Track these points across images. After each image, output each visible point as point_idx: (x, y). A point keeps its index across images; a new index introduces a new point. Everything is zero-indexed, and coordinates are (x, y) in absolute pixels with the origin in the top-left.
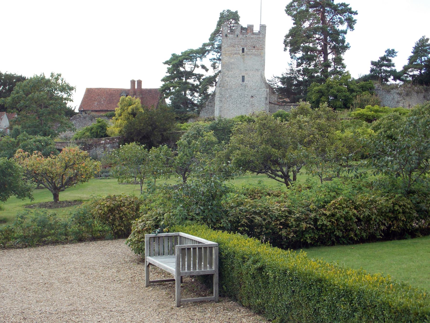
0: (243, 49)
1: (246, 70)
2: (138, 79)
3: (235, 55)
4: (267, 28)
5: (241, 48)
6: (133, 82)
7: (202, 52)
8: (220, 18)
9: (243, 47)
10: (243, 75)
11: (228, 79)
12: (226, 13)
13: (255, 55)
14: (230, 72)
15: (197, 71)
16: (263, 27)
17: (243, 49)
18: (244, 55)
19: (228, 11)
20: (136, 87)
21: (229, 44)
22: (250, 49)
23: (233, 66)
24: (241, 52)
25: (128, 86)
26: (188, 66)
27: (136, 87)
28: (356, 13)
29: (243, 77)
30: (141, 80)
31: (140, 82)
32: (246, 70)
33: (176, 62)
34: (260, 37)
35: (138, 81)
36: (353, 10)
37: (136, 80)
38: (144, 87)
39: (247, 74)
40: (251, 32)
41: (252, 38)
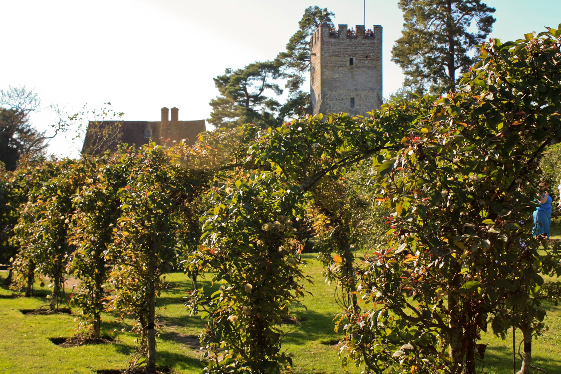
0: (351, 60)
1: (356, 90)
2: (172, 107)
3: (340, 69)
4: (383, 30)
5: (349, 59)
6: (165, 111)
7: (274, 68)
8: (305, 16)
9: (351, 57)
10: (352, 97)
11: (330, 102)
12: (313, 10)
13: (368, 68)
14: (334, 93)
15: (269, 94)
16: (378, 29)
17: (351, 60)
18: (352, 68)
19: (317, 8)
20: (170, 119)
21: (331, 52)
22: (361, 60)
23: (338, 84)
24: (348, 63)
25: (157, 117)
26: (253, 87)
27: (170, 119)
28: (493, 10)
29: (353, 100)
30: (177, 107)
31: (175, 111)
32: (356, 90)
34: (374, 43)
35: (172, 110)
36: (489, 6)
37: (170, 107)
38: (182, 117)
39: (357, 95)
40: (361, 35)
41: (363, 44)
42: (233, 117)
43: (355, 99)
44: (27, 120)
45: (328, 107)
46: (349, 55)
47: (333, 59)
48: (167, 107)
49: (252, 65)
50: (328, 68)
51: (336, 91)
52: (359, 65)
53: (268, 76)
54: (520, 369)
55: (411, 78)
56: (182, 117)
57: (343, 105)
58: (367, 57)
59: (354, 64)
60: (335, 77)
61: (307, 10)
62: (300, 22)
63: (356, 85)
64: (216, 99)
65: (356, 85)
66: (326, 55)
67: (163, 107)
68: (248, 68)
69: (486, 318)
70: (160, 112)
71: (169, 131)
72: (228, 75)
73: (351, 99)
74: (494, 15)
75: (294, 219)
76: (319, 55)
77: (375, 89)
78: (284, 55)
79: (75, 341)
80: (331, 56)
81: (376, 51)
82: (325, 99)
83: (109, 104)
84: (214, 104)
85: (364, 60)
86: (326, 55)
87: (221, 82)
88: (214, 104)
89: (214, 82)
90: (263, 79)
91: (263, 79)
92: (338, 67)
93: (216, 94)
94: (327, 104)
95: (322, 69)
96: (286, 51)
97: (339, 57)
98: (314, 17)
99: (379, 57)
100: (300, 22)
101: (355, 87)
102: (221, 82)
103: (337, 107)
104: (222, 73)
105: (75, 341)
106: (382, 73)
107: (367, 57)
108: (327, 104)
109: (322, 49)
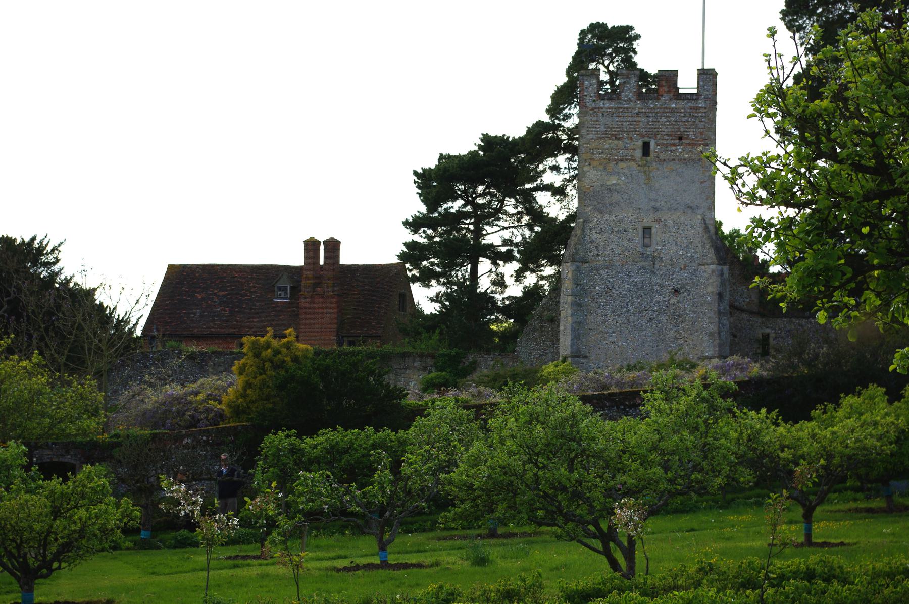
0: (646, 147)
1: (656, 209)
3: (621, 165)
5: (640, 143)
6: (311, 246)
9: (646, 139)
14: (607, 217)
16: (707, 77)
17: (646, 147)
20: (322, 262)
22: (667, 146)
23: (616, 197)
24: (638, 153)
25: (296, 259)
27: (322, 262)
29: (647, 230)
31: (333, 246)
32: (656, 209)
35: (325, 242)
37: (322, 237)
38: (346, 258)
39: (659, 221)
40: (669, 92)
41: (673, 111)
43: (654, 230)
44: (57, 261)
45: (593, 246)
46: (642, 136)
47: (607, 144)
50: (595, 163)
51: (610, 214)
52: (662, 157)
56: (346, 258)
57: (625, 243)
58: (680, 139)
59: (652, 155)
60: (608, 183)
63: (656, 201)
65: (656, 201)
66: (591, 136)
67: (307, 237)
70: (302, 247)
71: (319, 289)
73: (645, 228)
75: (708, 419)
77: (698, 207)
80: (601, 138)
81: (701, 125)
82: (587, 231)
85: (674, 145)
86: (591, 136)
92: (617, 162)
94: (592, 242)
96: (546, 118)
97: (619, 139)
98: (605, 42)
99: (710, 139)
101: (653, 204)
103: (613, 246)
106: (198, 266)
107: (680, 139)
108: (592, 242)
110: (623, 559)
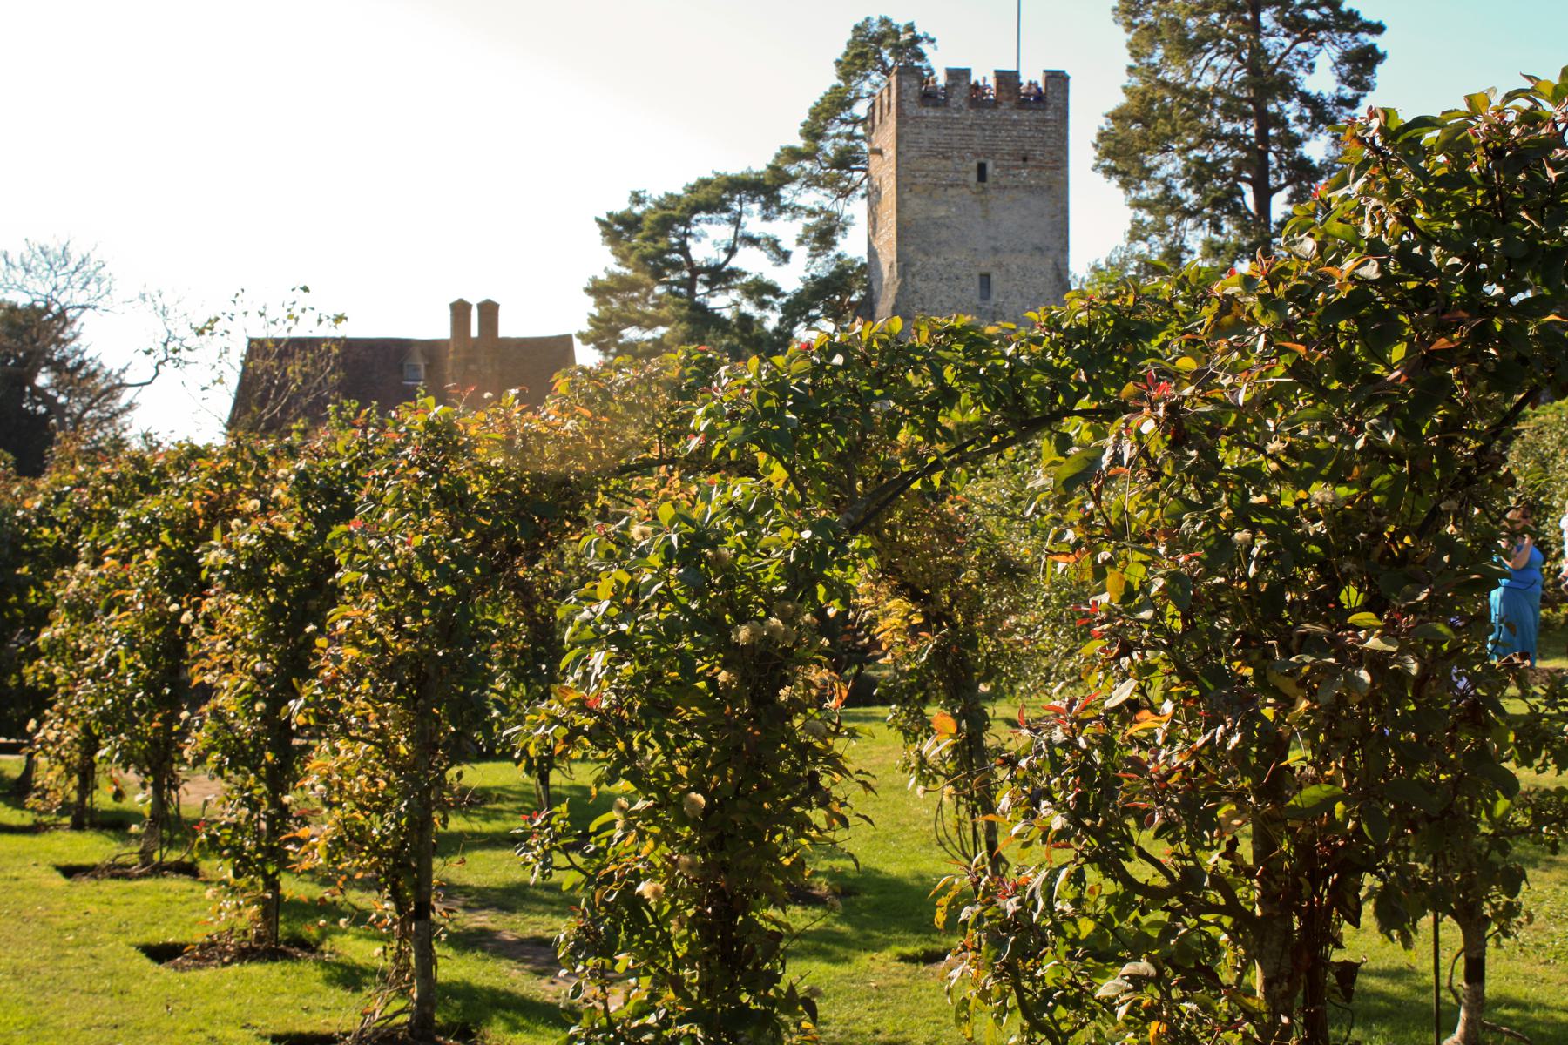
0: (982, 168)
1: (996, 250)
2: (482, 299)
3: (951, 192)
4: (1071, 83)
5: (974, 164)
6: (460, 310)
7: (765, 189)
9: (982, 160)
10: (985, 271)
11: (923, 285)
12: (875, 29)
13: (1030, 189)
14: (934, 259)
15: (752, 262)
16: (1058, 80)
17: (982, 168)
18: (985, 191)
19: (885, 21)
20: (474, 333)
21: (926, 144)
22: (1008, 168)
23: (945, 234)
24: (973, 177)
25: (438, 328)
26: (707, 242)
27: (474, 333)
28: (1378, 29)
29: (985, 280)
30: (494, 299)
31: (489, 311)
32: (996, 250)
33: (648, 236)
34: (1046, 121)
35: (482, 306)
36: (1367, 16)
37: (474, 300)
38: (510, 327)
39: (999, 266)
40: (1009, 99)
41: (1015, 123)
42: (650, 327)
43: (994, 278)
44: (76, 336)
45: (916, 298)
46: (977, 155)
47: (932, 164)
48: (467, 299)
49: (705, 183)
50: (917, 189)
51: (938, 255)
52: (1003, 182)
53: (750, 214)
54: (1453, 1030)
55: (1149, 218)
56: (510, 327)
57: (957, 294)
58: (1025, 159)
59: (990, 180)
60: (935, 215)
61: (857, 28)
62: (838, 63)
63: (995, 239)
64: (603, 276)
65: (995, 239)
66: (911, 154)
67: (455, 299)
68: (692, 189)
69: (1359, 888)
70: (448, 312)
71: (472, 367)
72: (638, 210)
73: (981, 275)
74: (1381, 42)
76: (890, 153)
77: (1048, 249)
78: (794, 155)
79: (209, 953)
80: (924, 157)
81: (1050, 142)
82: (909, 278)
83: (306, 289)
84: (598, 290)
85: (1017, 167)
86: (911, 154)
87: (619, 229)
88: (598, 290)
89: (598, 230)
90: (736, 222)
91: (736, 222)
92: (946, 187)
93: (603, 262)
94: (915, 292)
95: (899, 194)
96: (800, 143)
97: (947, 158)
98: (879, 48)
99: (1060, 160)
100: (838, 63)
101: (992, 243)
102: (619, 229)
103: (943, 298)
104: (621, 205)
105: (209, 953)
106: (1067, 203)
107: (1025, 159)
108: (915, 292)
109: (899, 137)
110: (488, 782)
